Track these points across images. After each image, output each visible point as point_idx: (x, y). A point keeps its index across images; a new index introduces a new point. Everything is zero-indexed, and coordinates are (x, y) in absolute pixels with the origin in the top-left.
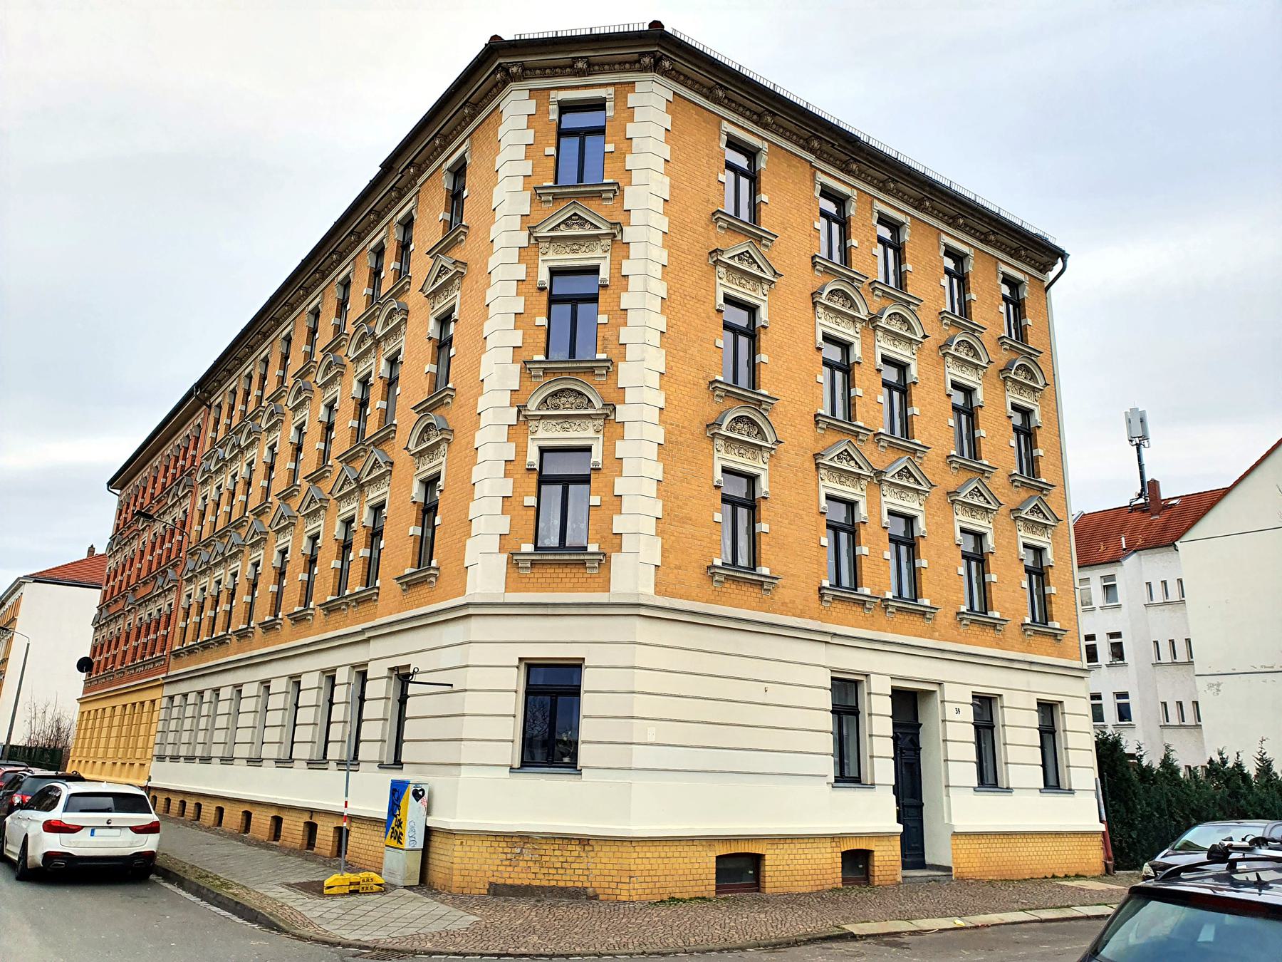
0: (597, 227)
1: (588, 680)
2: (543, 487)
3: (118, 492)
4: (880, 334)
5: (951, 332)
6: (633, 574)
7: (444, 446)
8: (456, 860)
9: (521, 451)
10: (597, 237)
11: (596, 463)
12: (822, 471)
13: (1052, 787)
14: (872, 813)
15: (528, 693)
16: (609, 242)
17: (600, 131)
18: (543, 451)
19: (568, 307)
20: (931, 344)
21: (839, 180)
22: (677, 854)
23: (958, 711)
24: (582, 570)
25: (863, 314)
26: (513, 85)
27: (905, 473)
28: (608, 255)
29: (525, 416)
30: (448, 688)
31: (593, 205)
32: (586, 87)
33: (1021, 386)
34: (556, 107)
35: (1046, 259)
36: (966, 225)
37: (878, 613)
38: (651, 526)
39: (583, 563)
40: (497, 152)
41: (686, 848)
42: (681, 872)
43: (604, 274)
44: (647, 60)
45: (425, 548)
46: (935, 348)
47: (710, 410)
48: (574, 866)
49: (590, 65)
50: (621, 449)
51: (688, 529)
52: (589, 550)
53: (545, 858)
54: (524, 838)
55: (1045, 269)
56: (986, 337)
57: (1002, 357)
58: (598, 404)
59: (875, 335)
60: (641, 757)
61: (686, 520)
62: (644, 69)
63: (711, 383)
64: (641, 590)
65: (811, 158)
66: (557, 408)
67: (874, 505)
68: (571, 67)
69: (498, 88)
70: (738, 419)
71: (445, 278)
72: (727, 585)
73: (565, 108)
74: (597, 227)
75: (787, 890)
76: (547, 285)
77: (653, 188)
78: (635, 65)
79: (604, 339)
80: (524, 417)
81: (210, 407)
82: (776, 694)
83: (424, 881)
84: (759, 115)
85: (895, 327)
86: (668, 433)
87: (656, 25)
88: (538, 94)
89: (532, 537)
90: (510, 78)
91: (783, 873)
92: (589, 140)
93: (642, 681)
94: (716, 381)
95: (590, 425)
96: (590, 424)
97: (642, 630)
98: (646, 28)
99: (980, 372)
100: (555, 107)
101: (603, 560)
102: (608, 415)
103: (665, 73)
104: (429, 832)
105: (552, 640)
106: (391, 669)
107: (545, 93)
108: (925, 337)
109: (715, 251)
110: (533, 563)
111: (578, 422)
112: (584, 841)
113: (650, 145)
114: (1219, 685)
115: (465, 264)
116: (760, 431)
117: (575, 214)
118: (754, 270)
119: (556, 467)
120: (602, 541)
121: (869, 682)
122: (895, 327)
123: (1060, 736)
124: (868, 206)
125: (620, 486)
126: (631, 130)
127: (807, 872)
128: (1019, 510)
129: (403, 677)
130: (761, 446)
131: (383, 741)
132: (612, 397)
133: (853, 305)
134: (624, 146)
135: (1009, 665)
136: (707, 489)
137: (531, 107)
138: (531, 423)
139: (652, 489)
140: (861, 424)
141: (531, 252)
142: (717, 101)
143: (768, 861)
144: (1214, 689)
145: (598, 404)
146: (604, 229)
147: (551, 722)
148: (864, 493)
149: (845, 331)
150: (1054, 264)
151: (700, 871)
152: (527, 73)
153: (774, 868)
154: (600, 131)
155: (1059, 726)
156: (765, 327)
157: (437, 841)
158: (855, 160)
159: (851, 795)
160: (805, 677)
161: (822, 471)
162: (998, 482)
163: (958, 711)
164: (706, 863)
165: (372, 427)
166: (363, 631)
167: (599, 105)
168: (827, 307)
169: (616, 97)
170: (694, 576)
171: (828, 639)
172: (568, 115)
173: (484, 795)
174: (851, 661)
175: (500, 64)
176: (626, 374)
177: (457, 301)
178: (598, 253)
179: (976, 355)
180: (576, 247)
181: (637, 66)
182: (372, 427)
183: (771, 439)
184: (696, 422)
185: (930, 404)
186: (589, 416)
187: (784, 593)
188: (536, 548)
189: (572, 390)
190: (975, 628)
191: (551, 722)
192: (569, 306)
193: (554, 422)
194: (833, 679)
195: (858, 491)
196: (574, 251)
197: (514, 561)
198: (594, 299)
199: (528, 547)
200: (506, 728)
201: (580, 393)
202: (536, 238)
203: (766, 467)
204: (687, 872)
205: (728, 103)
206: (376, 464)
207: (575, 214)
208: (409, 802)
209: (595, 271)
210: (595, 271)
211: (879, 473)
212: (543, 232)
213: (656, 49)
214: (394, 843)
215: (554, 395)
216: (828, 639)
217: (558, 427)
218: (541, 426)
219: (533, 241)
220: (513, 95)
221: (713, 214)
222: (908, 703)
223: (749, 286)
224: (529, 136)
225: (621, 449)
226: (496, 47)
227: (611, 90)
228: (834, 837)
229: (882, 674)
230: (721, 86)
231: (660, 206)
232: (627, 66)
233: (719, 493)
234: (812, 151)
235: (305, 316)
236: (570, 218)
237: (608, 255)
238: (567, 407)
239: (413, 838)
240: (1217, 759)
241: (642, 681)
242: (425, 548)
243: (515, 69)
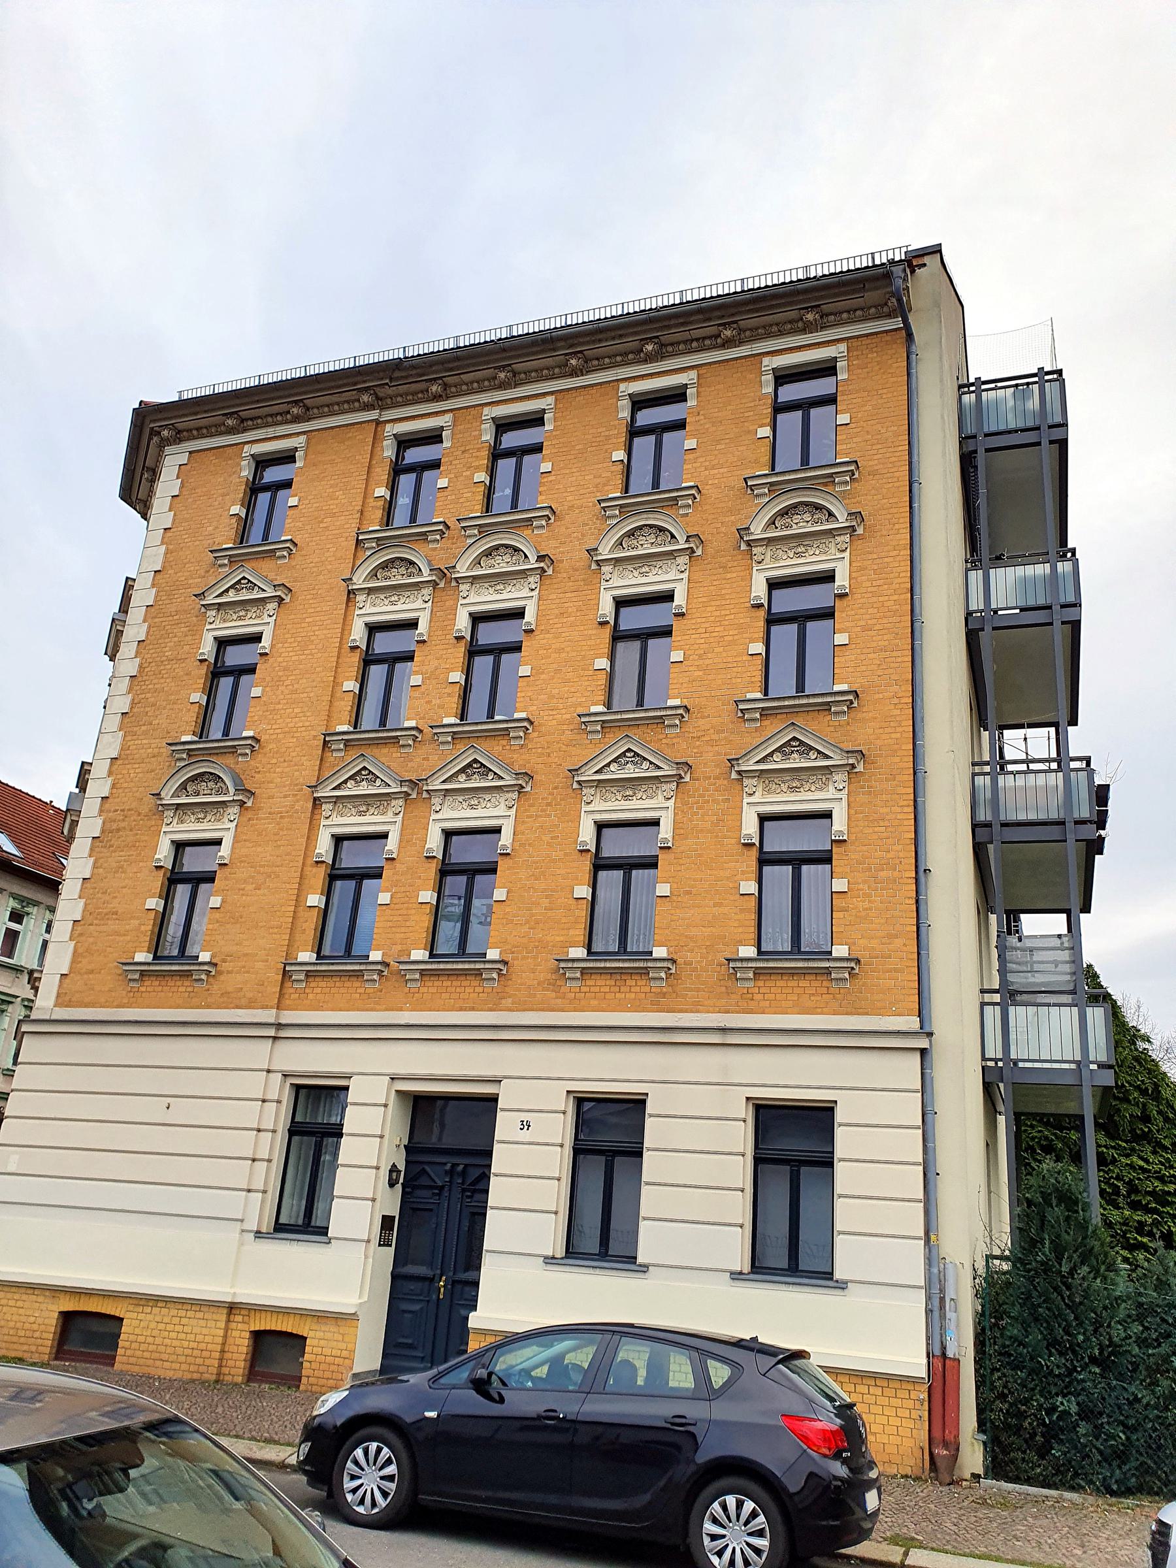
2: (765, 868)
10: (263, 600)
11: (504, 847)
15: (292, 1132)
16: (847, 538)
18: (600, 826)
19: (793, 628)
22: (11, 1303)
24: (476, 983)
26: (168, 450)
28: (685, 576)
32: (651, 375)
34: (770, 377)
39: (827, 971)
41: (24, 1297)
42: (12, 1324)
44: (650, 347)
52: (488, 957)
75: (146, 1370)
76: (765, 602)
82: (153, 1110)
89: (753, 936)
91: (143, 1347)
92: (667, 437)
95: (502, 800)
107: (473, 411)
110: (758, 973)
111: (487, 797)
119: (782, 840)
127: (179, 1351)
138: (746, 782)
151: (35, 1327)
152: (179, 437)
153: (132, 1338)
154: (680, 425)
169: (699, 385)
172: (786, 387)
188: (760, 952)
192: (491, 658)
196: (798, 555)
204: (19, 1325)
210: (828, 577)
217: (465, 805)
236: (239, 582)
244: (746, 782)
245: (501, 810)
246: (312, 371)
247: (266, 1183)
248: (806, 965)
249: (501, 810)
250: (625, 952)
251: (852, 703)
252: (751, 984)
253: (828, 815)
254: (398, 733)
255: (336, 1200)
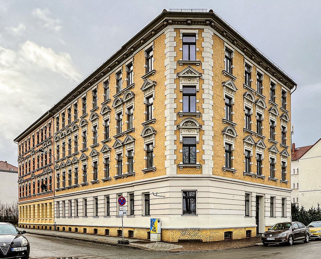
0: (195, 74)
1: (198, 195)
3: (17, 143)
4: (257, 106)
5: (271, 106)
6: (207, 170)
7: (153, 135)
8: (170, 235)
9: (178, 138)
10: (196, 77)
12: (245, 143)
13: (272, 216)
14: (251, 223)
17: (194, 44)
20: (267, 109)
21: (249, 61)
23: (268, 200)
25: (254, 101)
27: (261, 144)
28: (198, 82)
29: (179, 128)
30: (164, 197)
31: (194, 67)
33: (273, 114)
35: (292, 86)
36: (254, 59)
37: (254, 178)
38: (211, 158)
39: (196, 167)
40: (165, 48)
43: (198, 88)
45: (150, 162)
46: (267, 111)
47: (223, 126)
48: (197, 235)
49: (192, 22)
50: (204, 137)
51: (219, 159)
53: (190, 234)
54: (186, 229)
55: (291, 88)
56: (278, 107)
57: (281, 113)
58: (198, 125)
59: (256, 107)
60: (211, 212)
61: (218, 156)
62: (206, 25)
63: (223, 120)
64: (210, 173)
65: (243, 54)
66: (187, 126)
67: (254, 151)
68: (186, 22)
69: (163, 26)
70: (229, 130)
71: (149, 86)
72: (226, 172)
73: (185, 35)
74: (195, 74)
77: (210, 63)
78: (204, 23)
79: (198, 107)
80: (178, 128)
81: (54, 118)
82: (231, 197)
83: (162, 241)
84: (233, 40)
85: (260, 104)
86: (214, 133)
87: (211, 11)
88: (176, 30)
90: (169, 24)
93: (211, 195)
94: (224, 119)
95: (196, 131)
96: (195, 130)
97: (210, 183)
98: (208, 12)
99: (276, 117)
100: (181, 35)
101: (201, 167)
102: (200, 129)
103: (212, 26)
104: (161, 229)
105: (189, 185)
106: (143, 193)
107: (178, 30)
108: (266, 107)
109: (224, 82)
110: (184, 167)
111: (192, 130)
112: (199, 230)
113: (208, 50)
114: (304, 194)
115: (156, 82)
116: (233, 133)
117: (189, 70)
118: (231, 88)
120: (200, 161)
121: (252, 194)
122: (260, 104)
123: (274, 204)
124: (256, 69)
125: (204, 147)
126: (204, 44)
128: (270, 149)
129: (147, 196)
130: (233, 137)
131: (128, 211)
132: (201, 123)
133: (252, 99)
134: (201, 49)
135: (277, 190)
136: (222, 148)
137: (175, 34)
138: (180, 130)
139: (211, 148)
140: (252, 131)
141: (178, 81)
142: (223, 36)
143: (234, 233)
144: (303, 195)
145: (198, 125)
146: (197, 75)
147: (189, 203)
148: (252, 149)
149: (250, 105)
150: (293, 87)
152: (174, 23)
155: (274, 202)
156: (234, 104)
157: (164, 232)
158: (254, 56)
159: (248, 219)
160: (240, 191)
161: (245, 143)
162: (266, 141)
163: (268, 200)
164: (222, 233)
165: (124, 129)
166: (132, 184)
167: (194, 35)
168: (246, 99)
170: (220, 170)
171: (245, 184)
173: (174, 221)
174: (249, 189)
175: (167, 19)
176: (205, 117)
177: (154, 93)
178: (196, 82)
179: (276, 113)
180: (190, 80)
181: (205, 23)
182: (124, 129)
183: (235, 135)
184: (220, 131)
185: (266, 126)
186: (195, 128)
187: (237, 174)
189: (190, 121)
190: (272, 181)
191: (189, 203)
193: (186, 130)
194: (245, 194)
195: (251, 148)
196: (189, 81)
197: (179, 166)
198: (195, 95)
199: (182, 163)
200: (180, 206)
201: (193, 122)
202: (179, 76)
203: (234, 142)
205: (226, 37)
206: (129, 139)
207: (189, 70)
208: (156, 222)
209: (195, 87)
210: (195, 87)
211: (256, 144)
212: (181, 75)
213: (210, 19)
214: (154, 232)
215: (186, 122)
216: (245, 184)
218: (183, 131)
219: (178, 77)
220: (169, 30)
221: (223, 71)
222: (258, 198)
223: (230, 92)
224: (175, 44)
225: (204, 137)
226: (165, 14)
227: (197, 31)
228: (245, 228)
229: (255, 191)
230: (236, 40)
231: (211, 68)
232: (202, 23)
233: (225, 149)
234: (244, 52)
235: (91, 91)
236: (188, 71)
237: (198, 82)
238: (189, 125)
239: (158, 231)
240: (311, 209)
241: (211, 195)
242: (150, 162)
243: (170, 21)
244: (180, 130)
245: (196, 133)
246: (172, 11)
247: (252, 212)
248: (194, 166)
249: (196, 133)
250: (190, 163)
251: (200, 115)
252: (182, 169)
253: (195, 137)
254: (196, 114)
255: (87, 202)
